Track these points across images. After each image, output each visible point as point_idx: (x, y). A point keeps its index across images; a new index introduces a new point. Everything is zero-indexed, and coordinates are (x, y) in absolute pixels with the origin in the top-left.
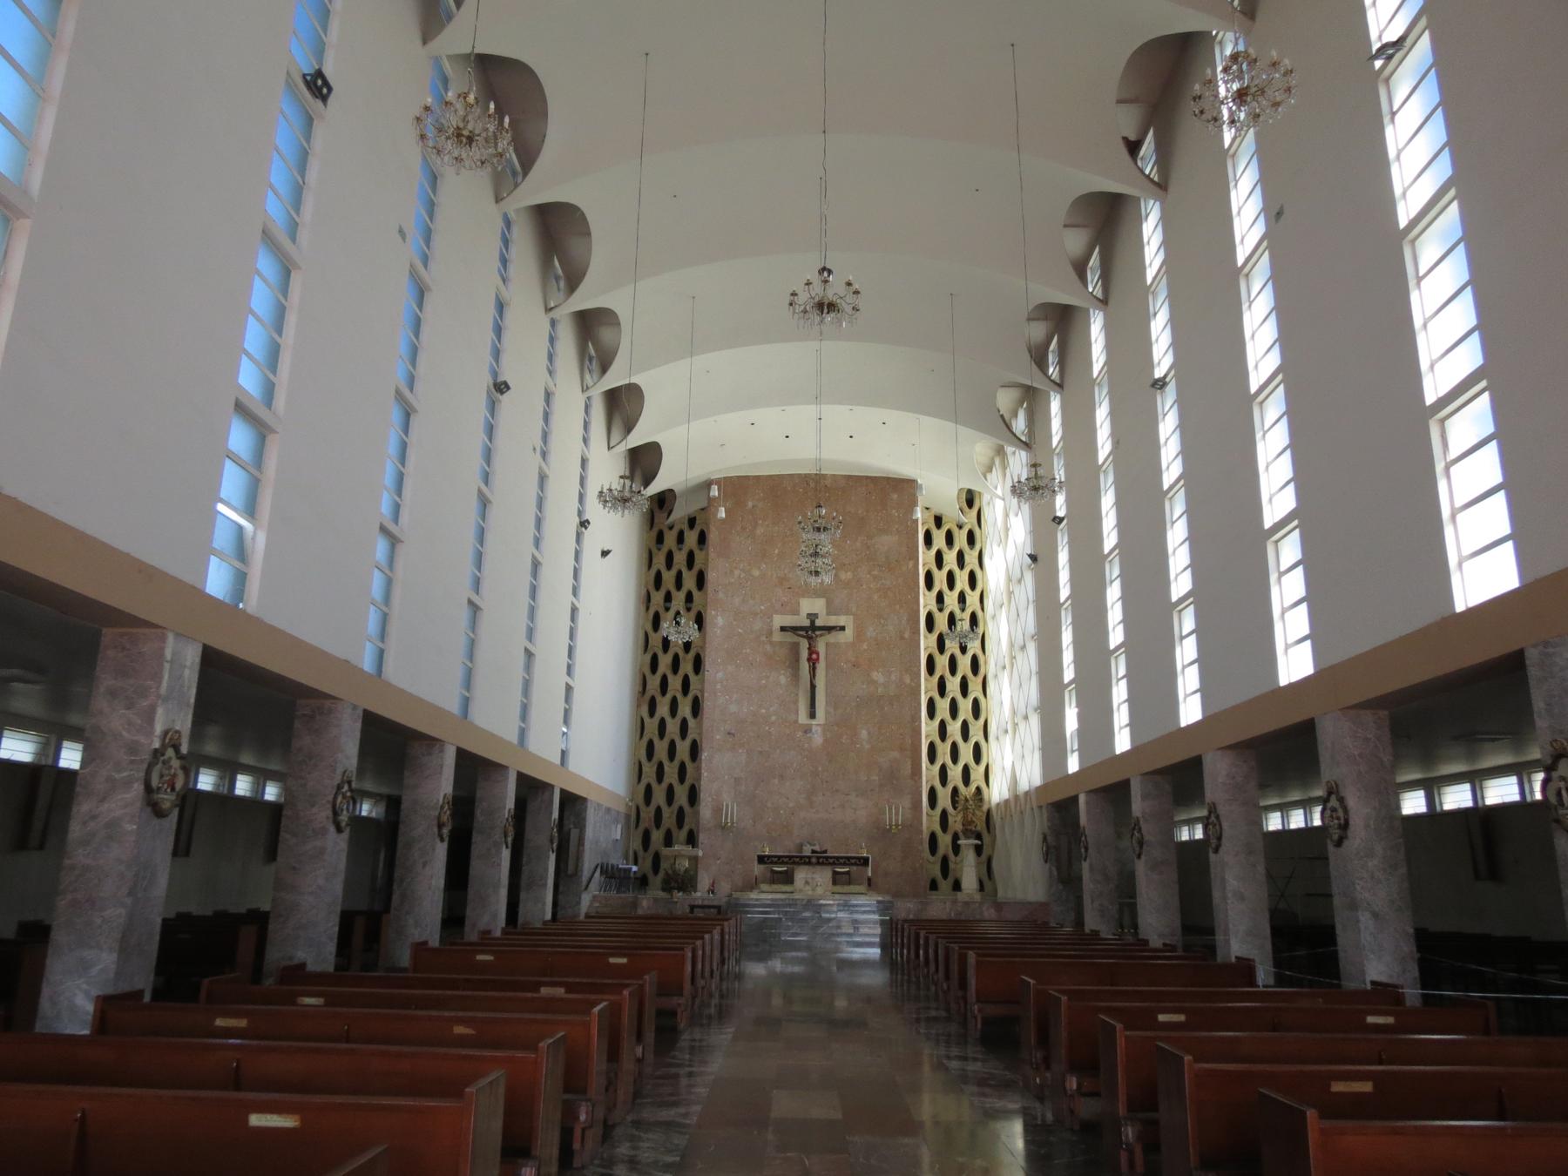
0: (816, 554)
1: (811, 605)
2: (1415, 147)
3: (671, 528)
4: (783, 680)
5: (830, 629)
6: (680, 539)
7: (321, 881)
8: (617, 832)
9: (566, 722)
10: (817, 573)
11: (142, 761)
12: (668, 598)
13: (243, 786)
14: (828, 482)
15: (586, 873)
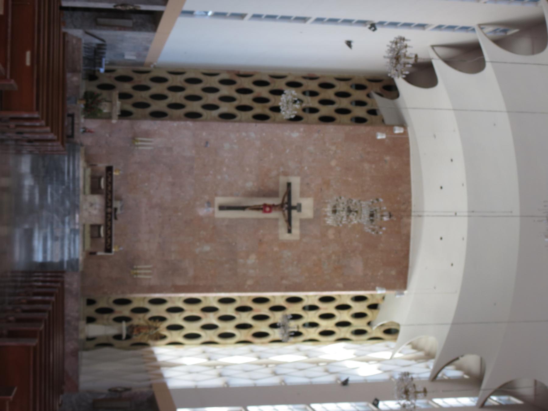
1: (307, 207)
3: (368, 96)
5: (289, 221)
8: (130, 56)
10: (334, 211)
14: (405, 220)
15: (97, 32)
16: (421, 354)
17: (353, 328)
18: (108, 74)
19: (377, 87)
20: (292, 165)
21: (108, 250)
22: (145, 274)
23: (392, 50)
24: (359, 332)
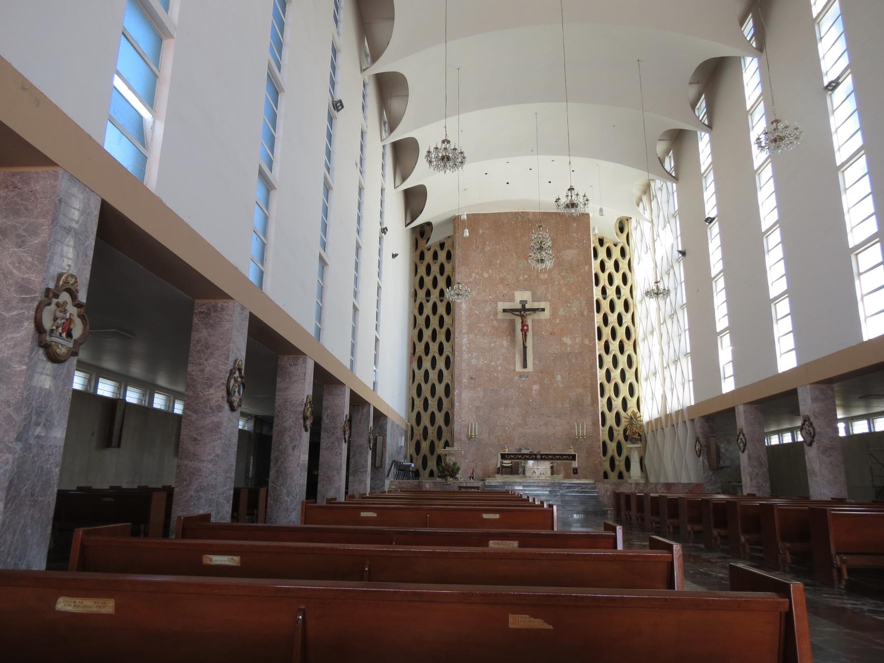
0: (541, 248)
1: (522, 296)
2: (832, 53)
3: (429, 250)
4: (505, 343)
5: (534, 310)
6: (435, 256)
7: (218, 451)
8: (402, 442)
9: (375, 363)
10: (542, 261)
11: (33, 299)
12: (428, 294)
13: (159, 402)
14: (530, 217)
15: (387, 467)
16: (645, 198)
17: (620, 258)
18: (414, 461)
19: (422, 243)
20: (488, 308)
21: (573, 457)
22: (583, 429)
23: (437, 166)
24: (623, 253)
